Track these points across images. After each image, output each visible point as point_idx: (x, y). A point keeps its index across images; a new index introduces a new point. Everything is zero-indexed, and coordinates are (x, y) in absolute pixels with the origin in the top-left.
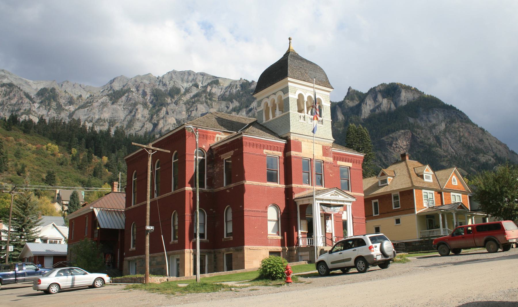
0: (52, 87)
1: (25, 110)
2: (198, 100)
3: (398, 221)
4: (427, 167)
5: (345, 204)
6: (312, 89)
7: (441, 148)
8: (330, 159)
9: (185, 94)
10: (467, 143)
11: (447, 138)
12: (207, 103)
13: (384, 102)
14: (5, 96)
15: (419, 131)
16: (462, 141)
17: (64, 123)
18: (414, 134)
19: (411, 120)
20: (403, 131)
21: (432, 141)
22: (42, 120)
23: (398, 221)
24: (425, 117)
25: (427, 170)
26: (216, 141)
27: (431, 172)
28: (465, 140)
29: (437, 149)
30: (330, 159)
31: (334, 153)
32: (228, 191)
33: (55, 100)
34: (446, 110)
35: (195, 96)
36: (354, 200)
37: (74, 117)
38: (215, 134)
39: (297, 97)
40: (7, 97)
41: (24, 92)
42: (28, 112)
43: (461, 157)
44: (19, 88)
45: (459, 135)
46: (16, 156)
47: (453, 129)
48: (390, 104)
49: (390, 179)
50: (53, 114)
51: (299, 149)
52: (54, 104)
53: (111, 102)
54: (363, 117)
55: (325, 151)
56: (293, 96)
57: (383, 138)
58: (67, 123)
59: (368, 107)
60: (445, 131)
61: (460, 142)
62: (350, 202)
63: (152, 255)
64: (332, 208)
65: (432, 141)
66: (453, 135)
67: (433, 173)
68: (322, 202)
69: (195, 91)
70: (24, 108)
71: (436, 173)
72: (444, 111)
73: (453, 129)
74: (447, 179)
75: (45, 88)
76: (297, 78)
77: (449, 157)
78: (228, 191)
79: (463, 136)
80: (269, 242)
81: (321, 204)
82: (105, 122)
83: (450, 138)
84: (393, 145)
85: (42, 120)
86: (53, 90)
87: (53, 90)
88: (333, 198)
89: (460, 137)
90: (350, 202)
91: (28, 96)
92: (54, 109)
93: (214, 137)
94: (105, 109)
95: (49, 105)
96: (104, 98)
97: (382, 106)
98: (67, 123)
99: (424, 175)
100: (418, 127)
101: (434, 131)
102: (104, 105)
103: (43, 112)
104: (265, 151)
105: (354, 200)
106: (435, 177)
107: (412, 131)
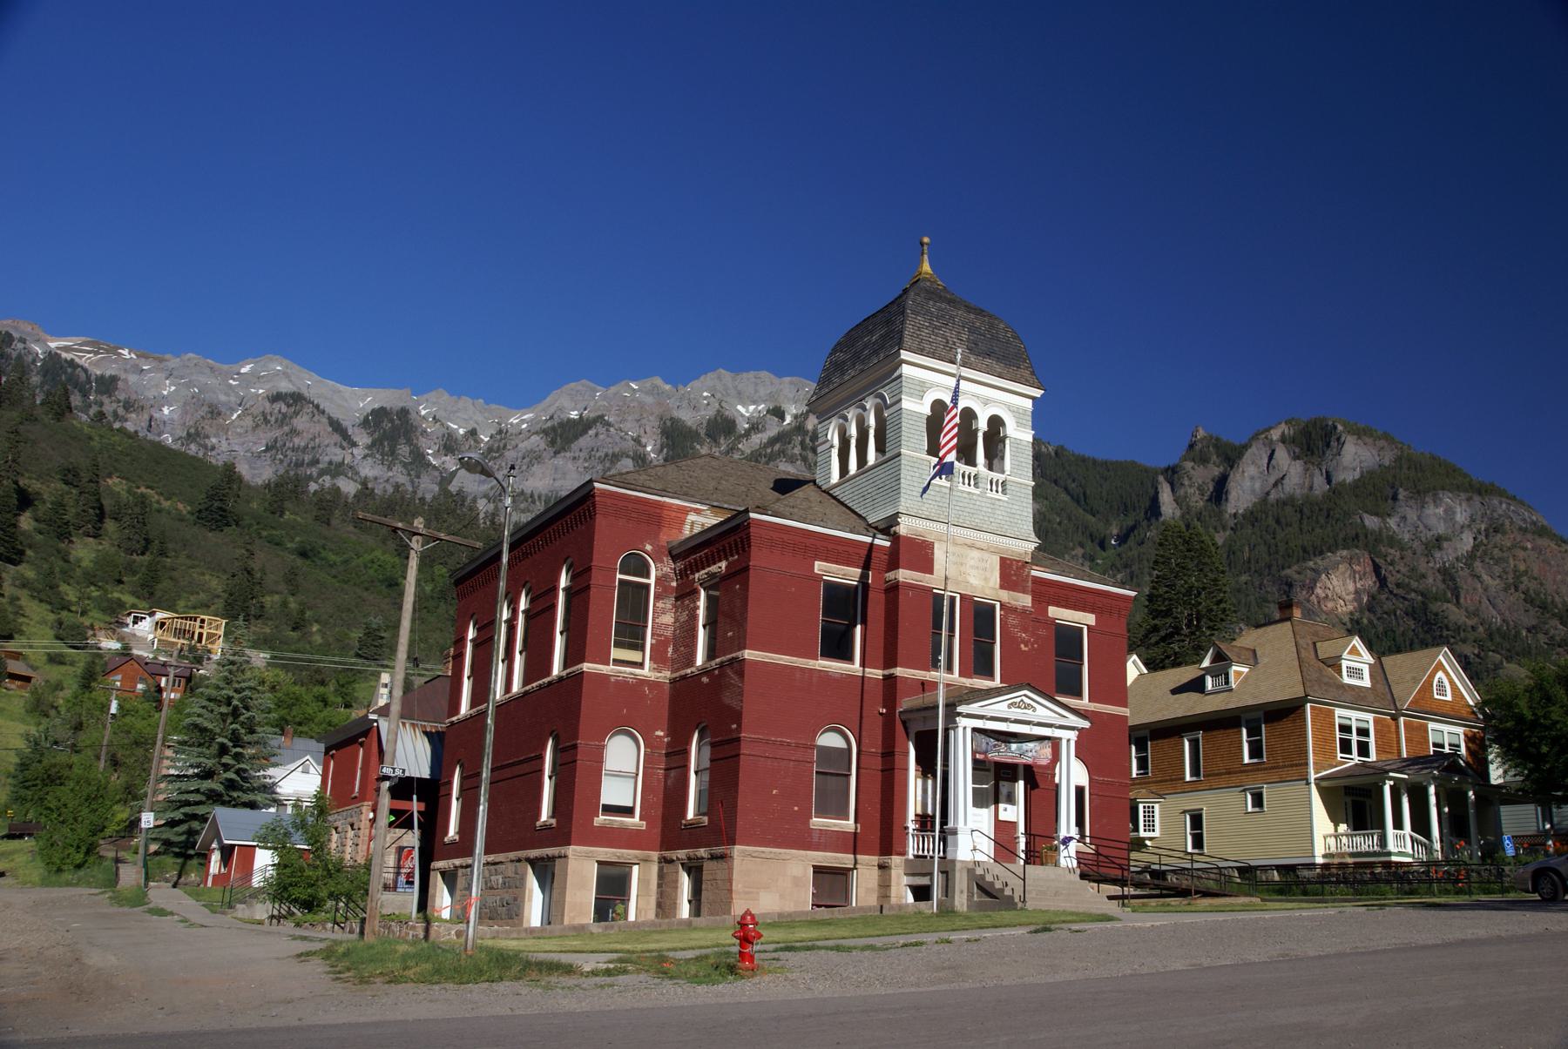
0: (401, 404)
1: (330, 463)
2: (782, 452)
3: (1258, 800)
4: (1356, 642)
5: (1057, 733)
6: (952, 382)
7: (1458, 604)
8: (1025, 600)
9: (747, 434)
10: (1538, 594)
11: (1479, 577)
12: (804, 459)
13: (1292, 471)
14: (281, 426)
15: (1394, 553)
16: (1522, 587)
17: (422, 499)
18: (1379, 561)
19: (1371, 522)
20: (1345, 553)
21: (1433, 582)
22: (366, 491)
23: (1258, 800)
24: (1412, 515)
25: (1354, 651)
26: (687, 532)
27: (1367, 657)
28: (1533, 586)
29: (1446, 605)
30: (1025, 600)
31: (1037, 580)
32: (705, 680)
33: (409, 442)
34: (1477, 498)
35: (772, 441)
36: (1086, 724)
37: (453, 488)
38: (686, 511)
39: (927, 411)
40: (286, 429)
41: (330, 418)
42: (337, 469)
43: (1518, 633)
44: (317, 407)
45: (1515, 571)
46: (289, 581)
47: (1496, 551)
48: (1312, 476)
49: (1238, 673)
50: (399, 475)
51: (927, 566)
52: (404, 450)
53: (551, 450)
54: (1231, 510)
55: (1011, 573)
56: (916, 407)
57: (1288, 572)
58: (429, 497)
59: (1248, 484)
60: (1471, 556)
61: (1516, 589)
62: (1072, 728)
63: (491, 858)
64: (1014, 746)
65: (1433, 582)
66: (1497, 570)
67: (1372, 661)
68: (979, 724)
69: (773, 430)
70: (327, 459)
71: (1387, 660)
72: (1469, 499)
73: (1496, 551)
74: (1416, 680)
75: (382, 409)
76: (933, 355)
77: (1481, 629)
78: (705, 680)
79: (1526, 572)
80: (816, 839)
81: (975, 730)
82: (534, 502)
83: (1485, 577)
84: (1318, 591)
85: (366, 491)
86: (404, 412)
87: (404, 412)
88: (1016, 713)
89: (1518, 575)
90: (1072, 728)
91: (336, 426)
92: (405, 465)
93: (683, 522)
94: (535, 468)
95: (393, 452)
96: (535, 438)
97: (1286, 481)
98: (429, 497)
99: (1344, 664)
100: (1393, 541)
101: (1438, 555)
102: (534, 457)
103: (368, 470)
104: (819, 566)
105: (1086, 724)
106: (1378, 672)
107: (1373, 552)
